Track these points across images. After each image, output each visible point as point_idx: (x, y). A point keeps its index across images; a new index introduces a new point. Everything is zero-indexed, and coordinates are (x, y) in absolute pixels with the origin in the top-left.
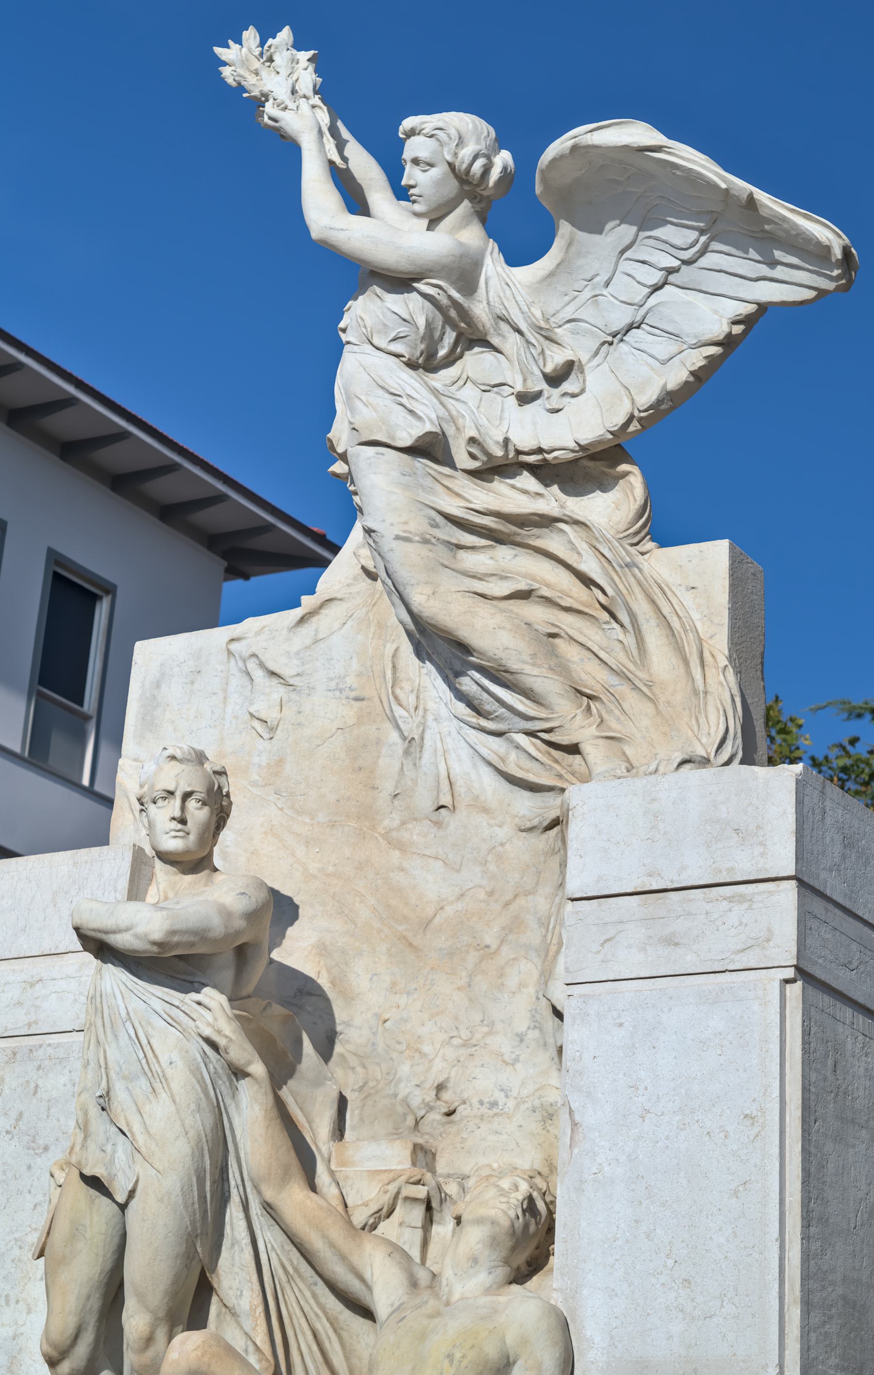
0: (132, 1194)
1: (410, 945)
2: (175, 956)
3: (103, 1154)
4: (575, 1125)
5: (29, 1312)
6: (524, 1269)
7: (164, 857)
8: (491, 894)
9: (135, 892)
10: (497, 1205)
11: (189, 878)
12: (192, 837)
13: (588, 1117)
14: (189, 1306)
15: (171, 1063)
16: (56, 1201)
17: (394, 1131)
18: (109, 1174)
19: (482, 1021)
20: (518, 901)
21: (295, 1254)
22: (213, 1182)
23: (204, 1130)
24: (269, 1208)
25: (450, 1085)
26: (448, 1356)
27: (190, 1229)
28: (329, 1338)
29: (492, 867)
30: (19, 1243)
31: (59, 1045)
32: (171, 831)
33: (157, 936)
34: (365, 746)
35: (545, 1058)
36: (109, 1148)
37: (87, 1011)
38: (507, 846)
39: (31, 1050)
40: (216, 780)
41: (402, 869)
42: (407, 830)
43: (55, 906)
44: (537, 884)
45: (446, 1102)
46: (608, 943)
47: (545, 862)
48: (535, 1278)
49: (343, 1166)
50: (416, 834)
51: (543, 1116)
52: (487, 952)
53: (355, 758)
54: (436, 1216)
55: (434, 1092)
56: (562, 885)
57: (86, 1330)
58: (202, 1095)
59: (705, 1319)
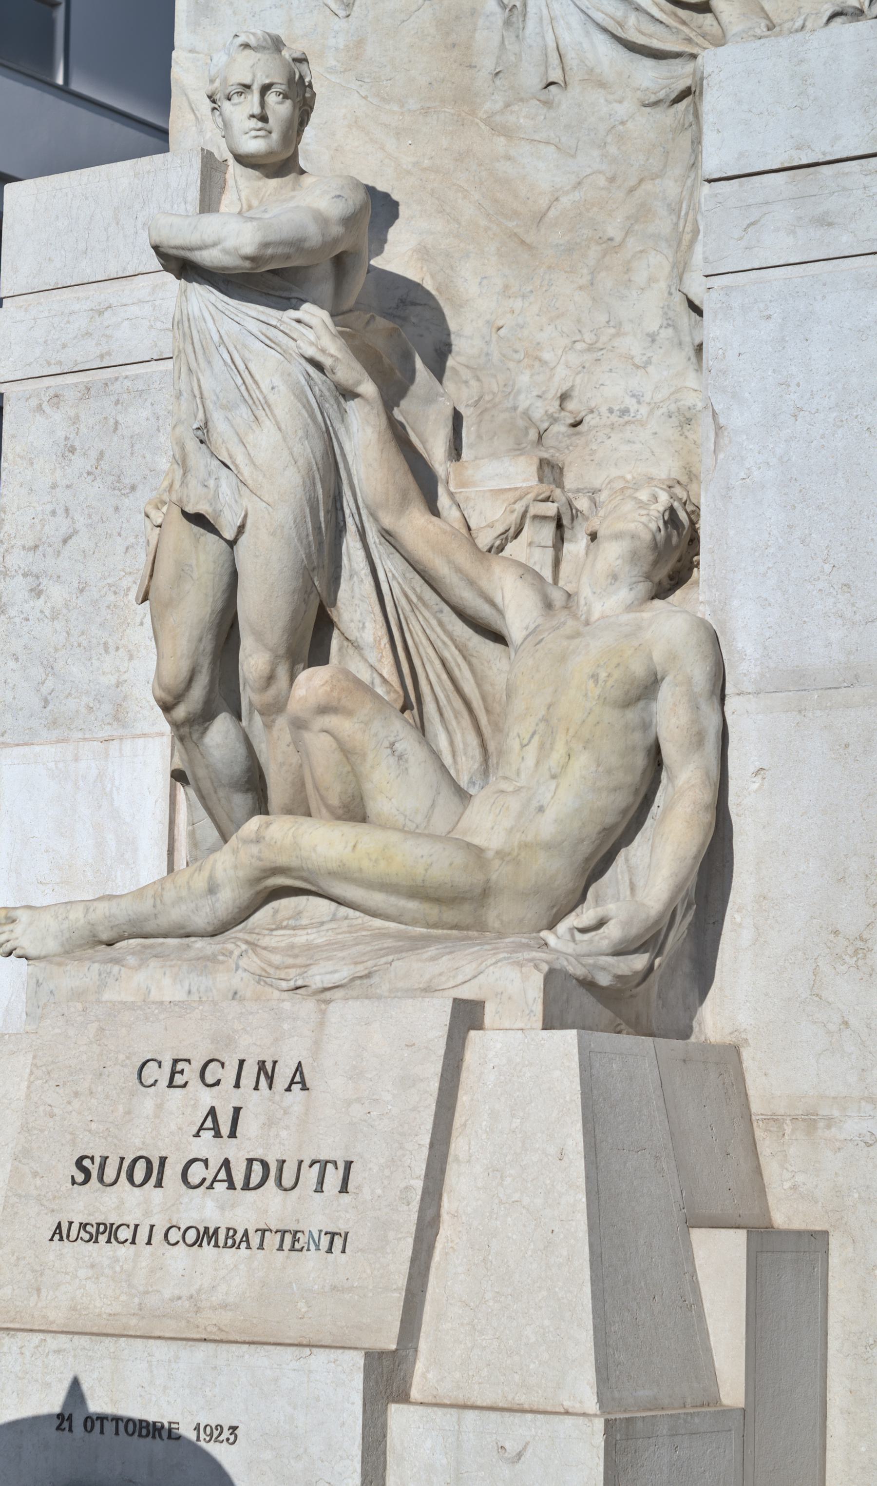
0: (241, 529)
1: (523, 242)
2: (268, 271)
3: (205, 490)
4: (719, 429)
5: (131, 658)
6: (666, 583)
7: (242, 160)
8: (612, 180)
9: (208, 202)
10: (637, 520)
11: (274, 182)
12: (275, 136)
13: (736, 419)
14: (309, 642)
15: (273, 388)
16: (155, 542)
17: (516, 447)
18: (214, 510)
19: (608, 322)
20: (643, 186)
21: (418, 581)
22: (327, 512)
23: (314, 458)
24: (387, 535)
25: (575, 393)
26: (593, 676)
27: (306, 562)
28: (459, 666)
29: (613, 150)
30: (113, 589)
31: (137, 377)
32: (251, 130)
33: (249, 249)
34: (458, 18)
35: (681, 358)
36: (212, 483)
37: (174, 337)
38: (630, 125)
39: (106, 384)
40: (297, 69)
41: (509, 158)
42: (512, 112)
43: (118, 224)
44: (665, 166)
45: (571, 412)
46: (752, 227)
47: (673, 139)
48: (678, 592)
49: (463, 487)
50: (523, 117)
51: (680, 422)
52: (610, 246)
53: (448, 33)
54: (567, 534)
55: (558, 403)
56: (694, 165)
57: (200, 672)
58: (309, 420)
59: (867, 623)
